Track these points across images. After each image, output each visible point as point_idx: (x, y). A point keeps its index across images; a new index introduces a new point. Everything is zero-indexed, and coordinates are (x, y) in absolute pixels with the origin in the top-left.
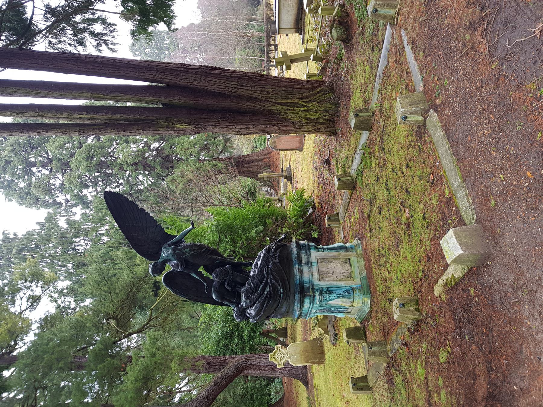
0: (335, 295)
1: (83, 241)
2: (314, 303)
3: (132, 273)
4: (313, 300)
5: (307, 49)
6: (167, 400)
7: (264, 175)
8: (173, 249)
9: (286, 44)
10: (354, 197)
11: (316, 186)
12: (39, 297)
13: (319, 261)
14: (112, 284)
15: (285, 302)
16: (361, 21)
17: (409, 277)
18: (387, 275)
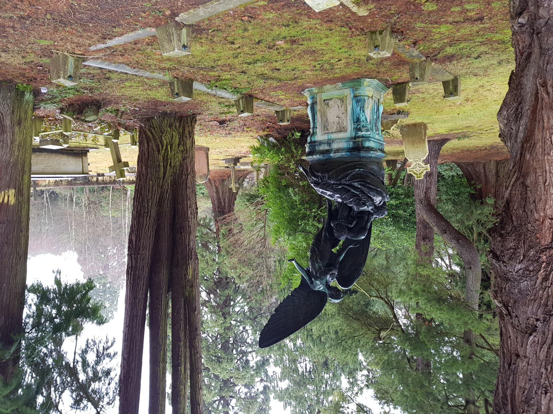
0: (361, 115)
1: (302, 364)
2: (370, 137)
3: (334, 315)
5: (105, 145)
6: (458, 278)
7: (233, 186)
9: (97, 165)
10: (260, 96)
11: (247, 134)
12: (359, 405)
13: (327, 131)
14: (346, 336)
15: (369, 166)
16: (78, 91)
17: (346, 40)
18: (342, 62)
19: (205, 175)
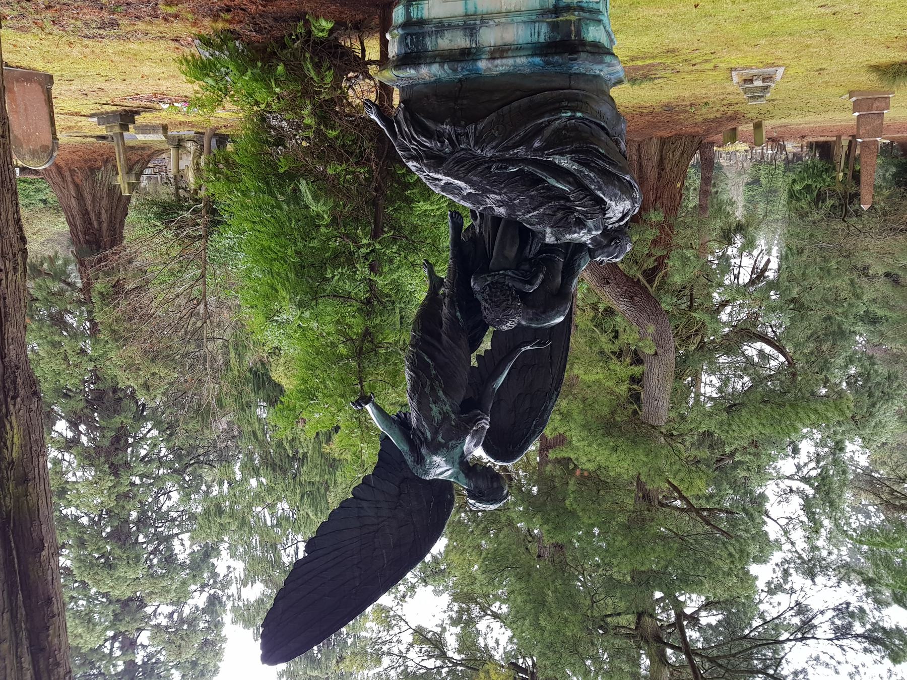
4: (590, 11)
7: (121, 181)
19: (44, 148)
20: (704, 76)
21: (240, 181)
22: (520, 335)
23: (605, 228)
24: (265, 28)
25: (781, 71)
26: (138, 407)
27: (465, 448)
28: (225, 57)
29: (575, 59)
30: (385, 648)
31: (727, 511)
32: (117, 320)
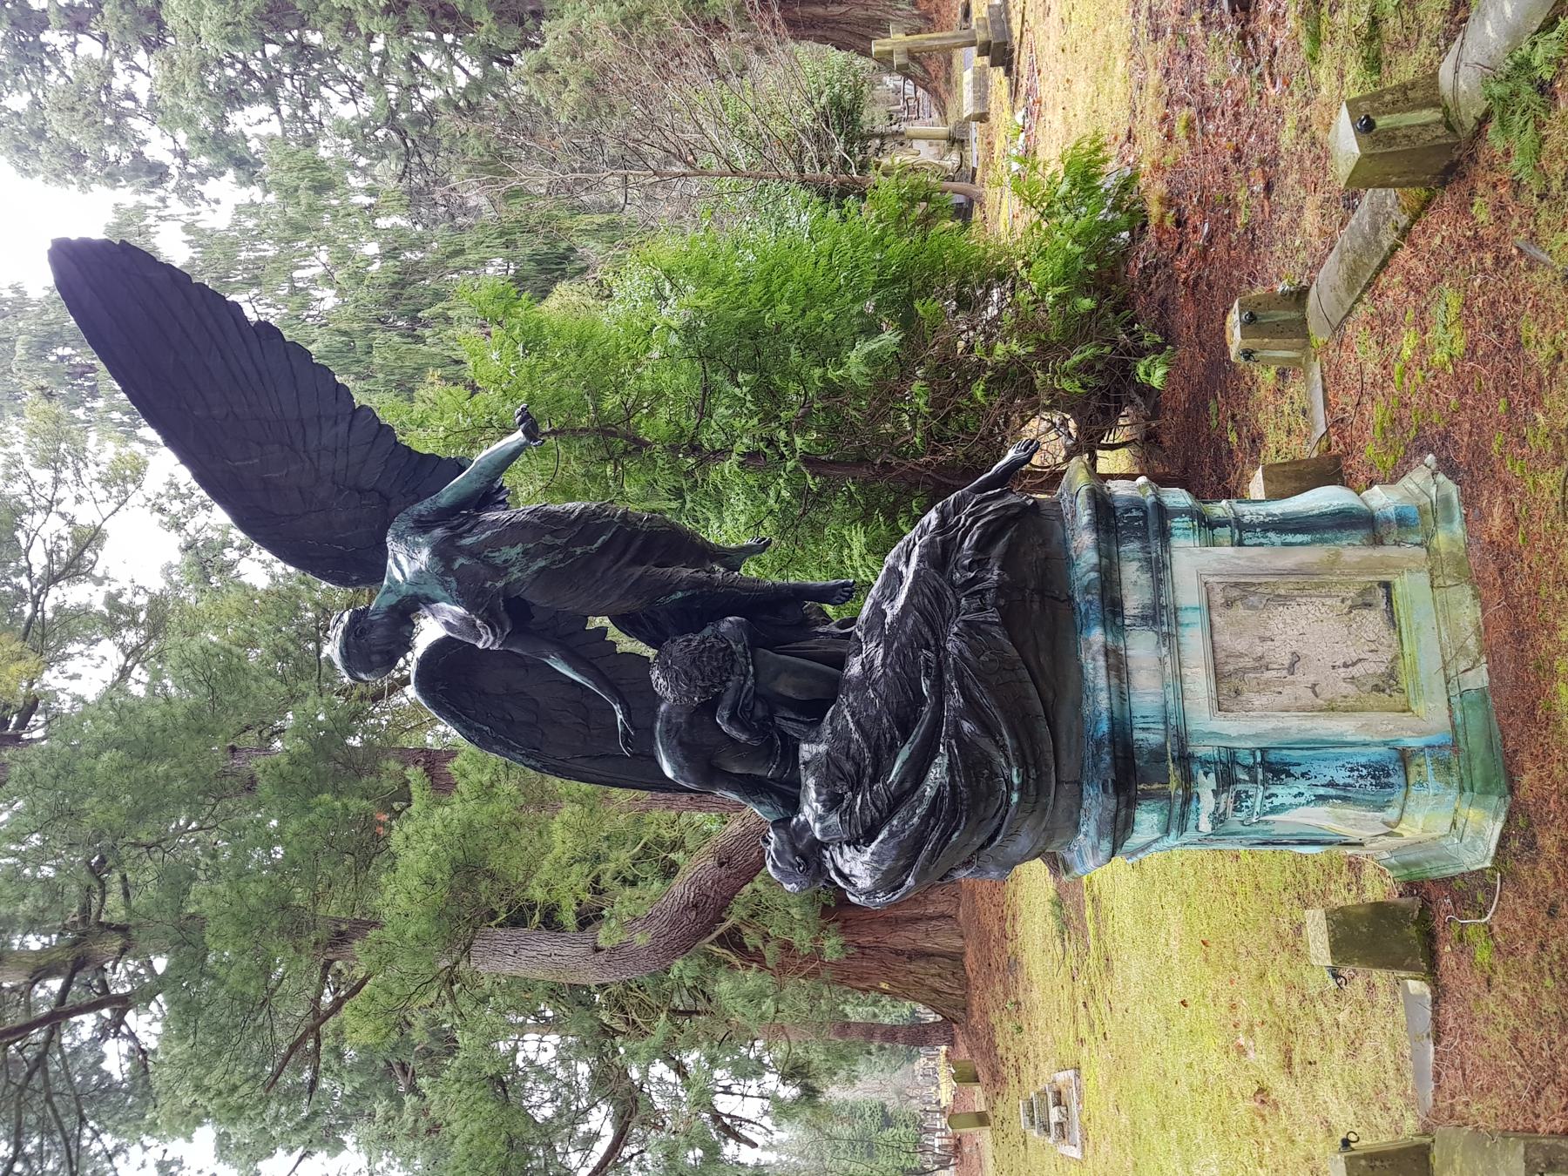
0: (1302, 785)
4: (1183, 816)
7: (896, 40)
8: (439, 552)
13: (1218, 599)
20: (1067, 1022)
21: (900, 235)
22: (641, 700)
23: (825, 846)
24: (1149, 283)
25: (1075, 1153)
26: (508, 53)
27: (443, 605)
28: (1103, 215)
29: (1105, 790)
30: (68, 474)
31: (314, 1083)
32: (659, 24)
